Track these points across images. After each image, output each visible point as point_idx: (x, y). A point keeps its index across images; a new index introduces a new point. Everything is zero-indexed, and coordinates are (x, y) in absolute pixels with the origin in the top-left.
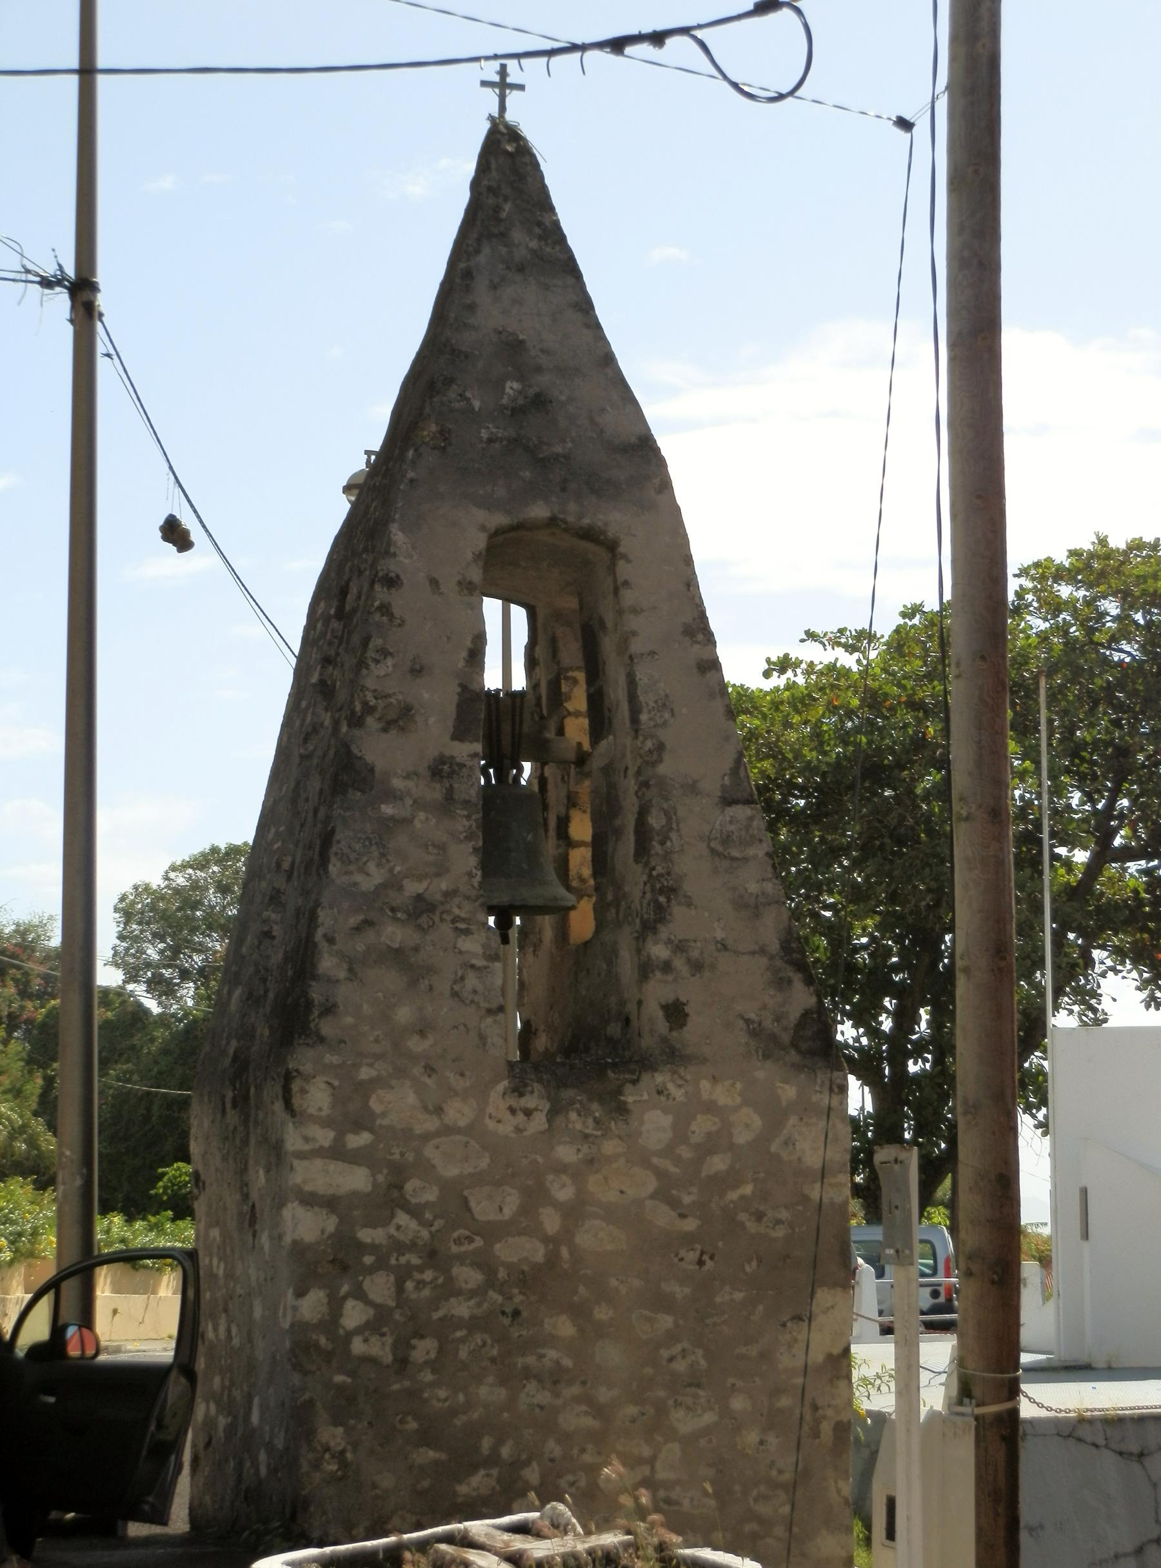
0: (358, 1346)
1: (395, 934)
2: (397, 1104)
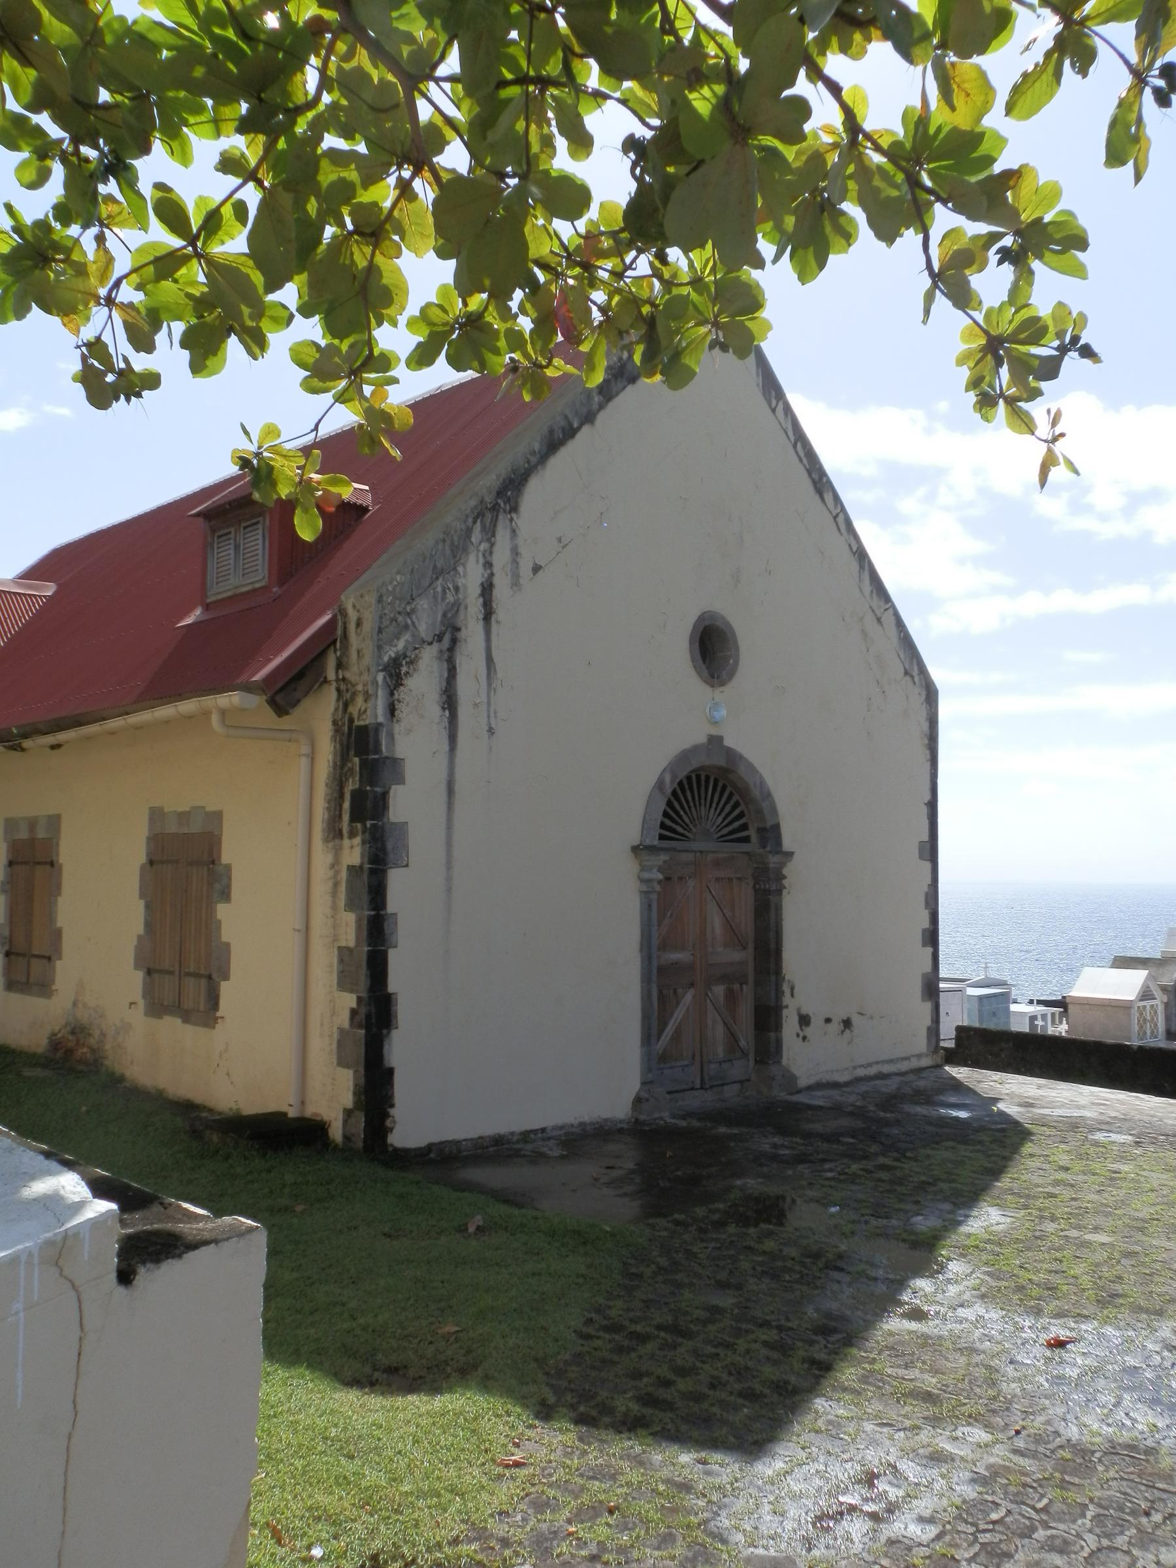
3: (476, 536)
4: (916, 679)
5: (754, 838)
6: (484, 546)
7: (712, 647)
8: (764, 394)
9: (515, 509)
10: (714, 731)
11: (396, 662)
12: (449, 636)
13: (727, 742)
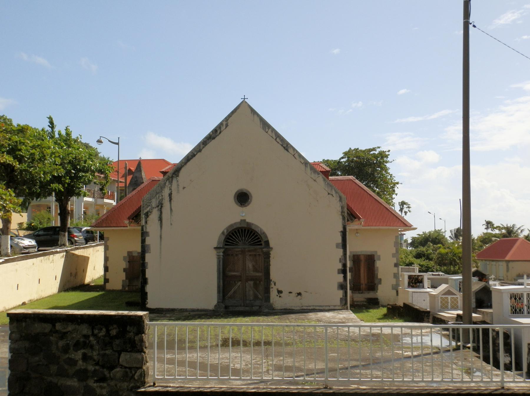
3: (167, 183)
4: (334, 195)
5: (263, 244)
6: (170, 185)
7: (243, 198)
8: (263, 129)
9: (178, 176)
10: (243, 218)
11: (147, 213)
12: (160, 206)
13: (247, 221)
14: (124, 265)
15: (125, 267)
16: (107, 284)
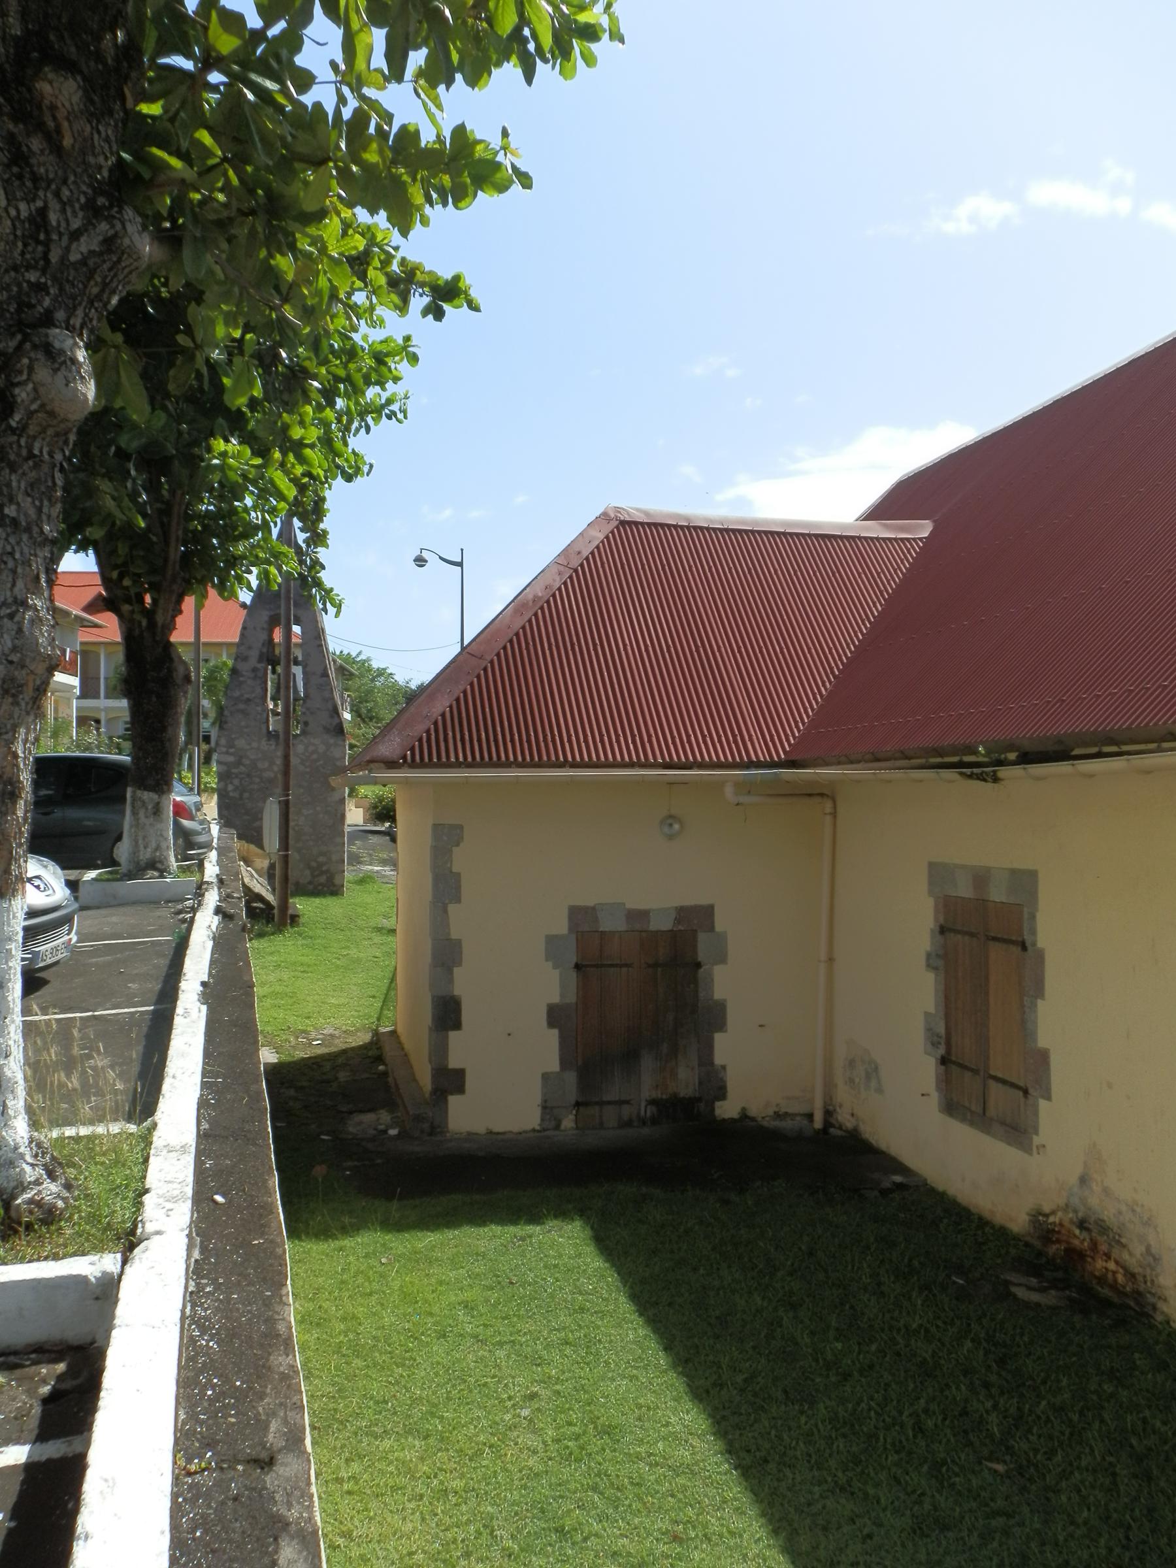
0: (231, 794)
1: (241, 706)
2: (241, 743)
14: (550, 985)
15: (556, 999)
16: (453, 1100)
